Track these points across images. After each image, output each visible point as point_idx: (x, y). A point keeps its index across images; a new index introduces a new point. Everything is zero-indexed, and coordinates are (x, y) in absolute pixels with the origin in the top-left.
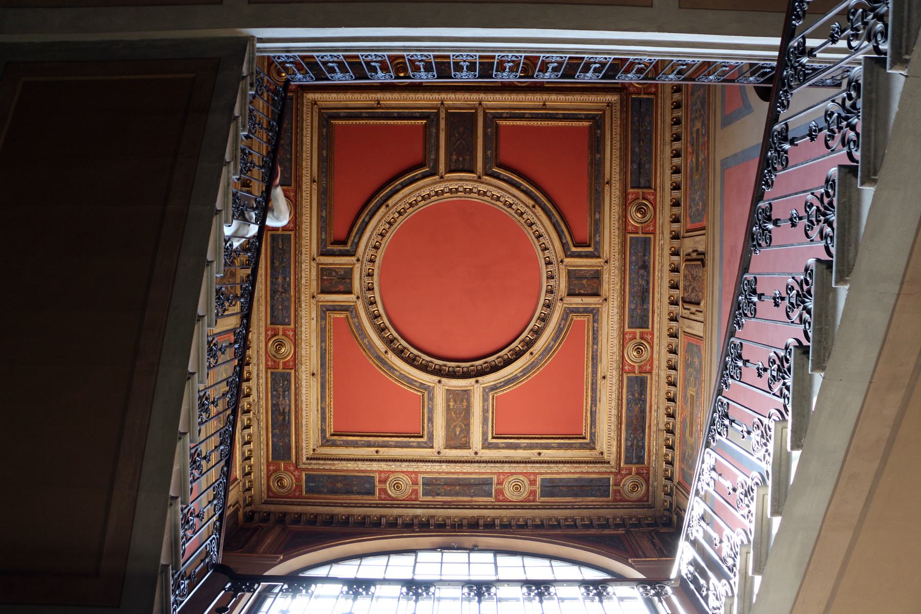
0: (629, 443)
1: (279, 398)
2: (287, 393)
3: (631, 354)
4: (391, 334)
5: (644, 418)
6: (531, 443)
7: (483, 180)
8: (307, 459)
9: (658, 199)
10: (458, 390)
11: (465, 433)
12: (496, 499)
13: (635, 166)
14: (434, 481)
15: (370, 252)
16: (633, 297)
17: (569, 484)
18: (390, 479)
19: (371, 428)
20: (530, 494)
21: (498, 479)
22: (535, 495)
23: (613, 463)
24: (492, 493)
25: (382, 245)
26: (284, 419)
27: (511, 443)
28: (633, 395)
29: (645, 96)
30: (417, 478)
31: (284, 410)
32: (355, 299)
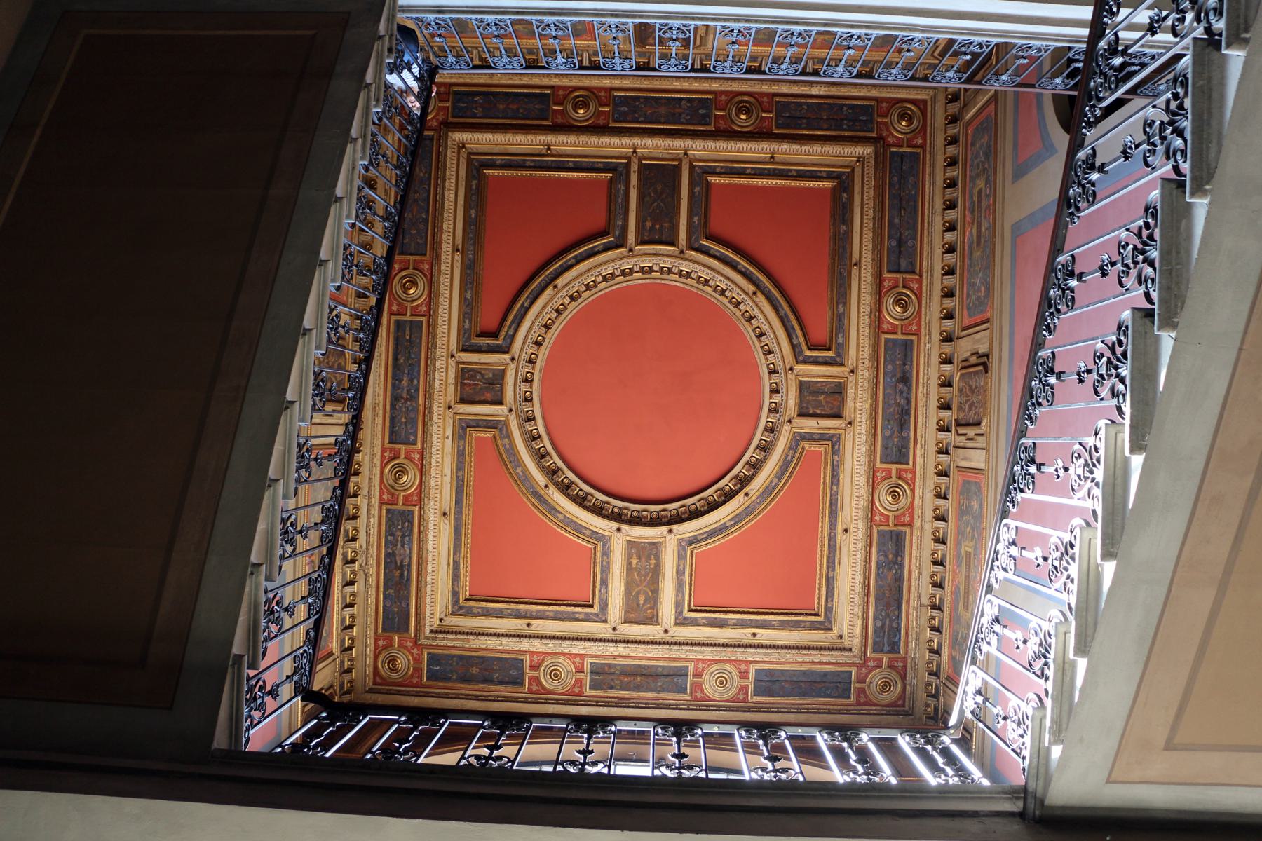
0: (879, 624)
1: (397, 545)
2: (407, 538)
3: (884, 499)
5: (900, 589)
6: (742, 620)
7: (686, 256)
8: (432, 631)
9: (924, 288)
13: (894, 243)
14: (606, 668)
15: (530, 349)
16: (888, 421)
17: (795, 679)
18: (546, 664)
19: (522, 592)
20: (739, 691)
21: (696, 669)
22: (746, 693)
23: (856, 650)
25: (547, 341)
26: (402, 575)
27: (716, 618)
28: (886, 556)
29: (909, 150)
30: (582, 664)
31: (402, 562)
32: (506, 412)
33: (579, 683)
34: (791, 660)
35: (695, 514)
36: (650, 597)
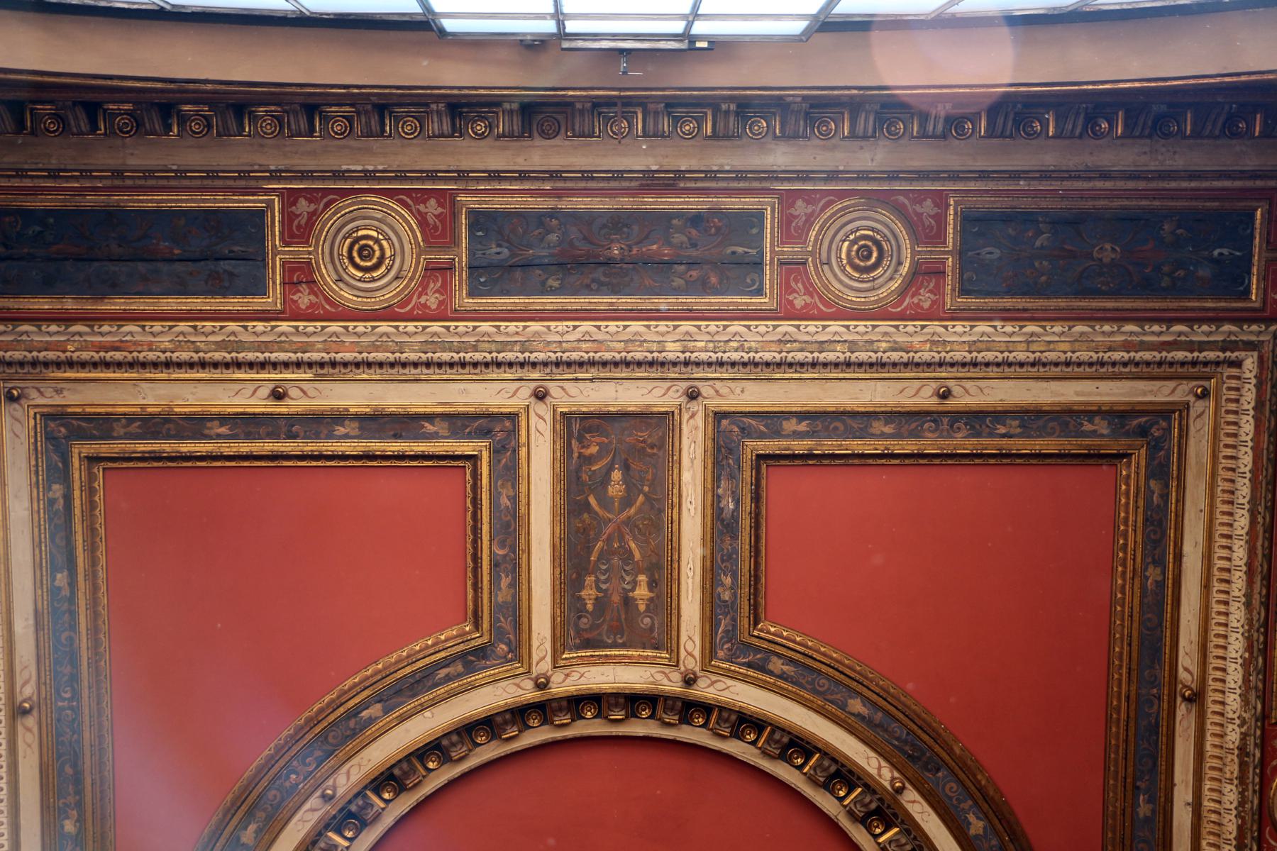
4: (876, 837)
8: (1238, 364)
10: (615, 645)
11: (585, 477)
12: (453, 203)
14: (714, 280)
17: (141, 267)
18: (895, 285)
19: (964, 478)
20: (310, 224)
21: (445, 289)
22: (288, 218)
24: (472, 227)
30: (786, 288)
33: (791, 230)
34: (158, 326)
35: (488, 725)
36: (592, 491)
